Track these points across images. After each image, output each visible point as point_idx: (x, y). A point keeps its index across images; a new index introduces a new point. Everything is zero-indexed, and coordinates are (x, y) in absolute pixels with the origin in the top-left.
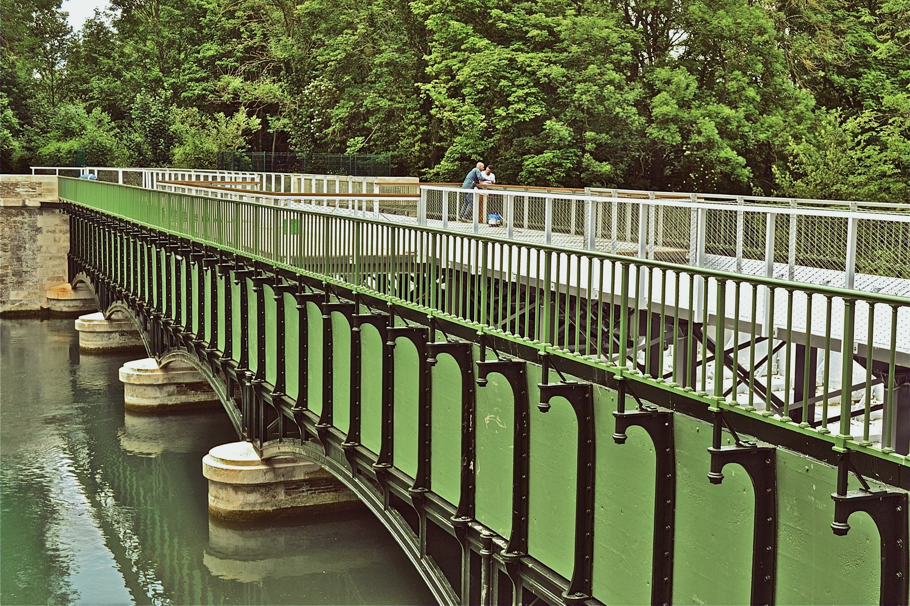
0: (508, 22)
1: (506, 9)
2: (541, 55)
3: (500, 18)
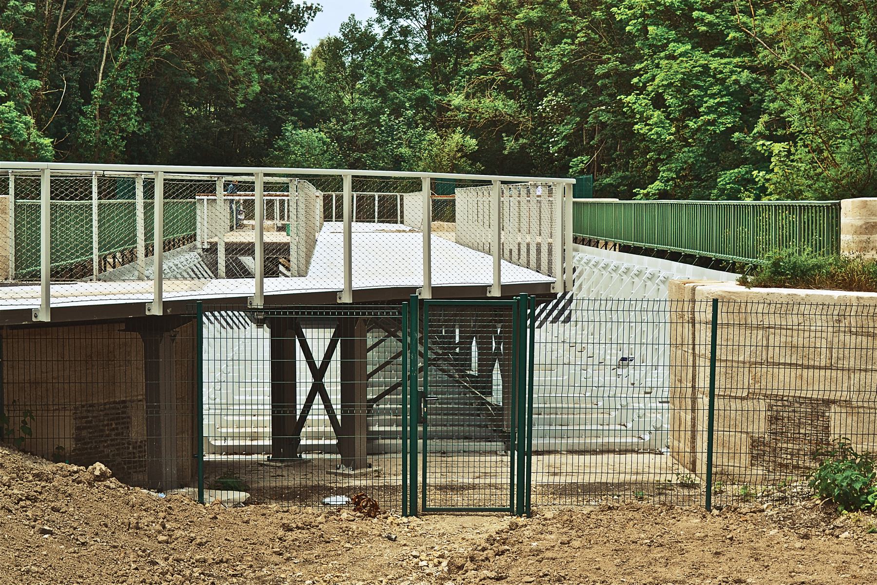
0: (710, 24)
1: (710, 10)
2: (737, 60)
3: (701, 20)
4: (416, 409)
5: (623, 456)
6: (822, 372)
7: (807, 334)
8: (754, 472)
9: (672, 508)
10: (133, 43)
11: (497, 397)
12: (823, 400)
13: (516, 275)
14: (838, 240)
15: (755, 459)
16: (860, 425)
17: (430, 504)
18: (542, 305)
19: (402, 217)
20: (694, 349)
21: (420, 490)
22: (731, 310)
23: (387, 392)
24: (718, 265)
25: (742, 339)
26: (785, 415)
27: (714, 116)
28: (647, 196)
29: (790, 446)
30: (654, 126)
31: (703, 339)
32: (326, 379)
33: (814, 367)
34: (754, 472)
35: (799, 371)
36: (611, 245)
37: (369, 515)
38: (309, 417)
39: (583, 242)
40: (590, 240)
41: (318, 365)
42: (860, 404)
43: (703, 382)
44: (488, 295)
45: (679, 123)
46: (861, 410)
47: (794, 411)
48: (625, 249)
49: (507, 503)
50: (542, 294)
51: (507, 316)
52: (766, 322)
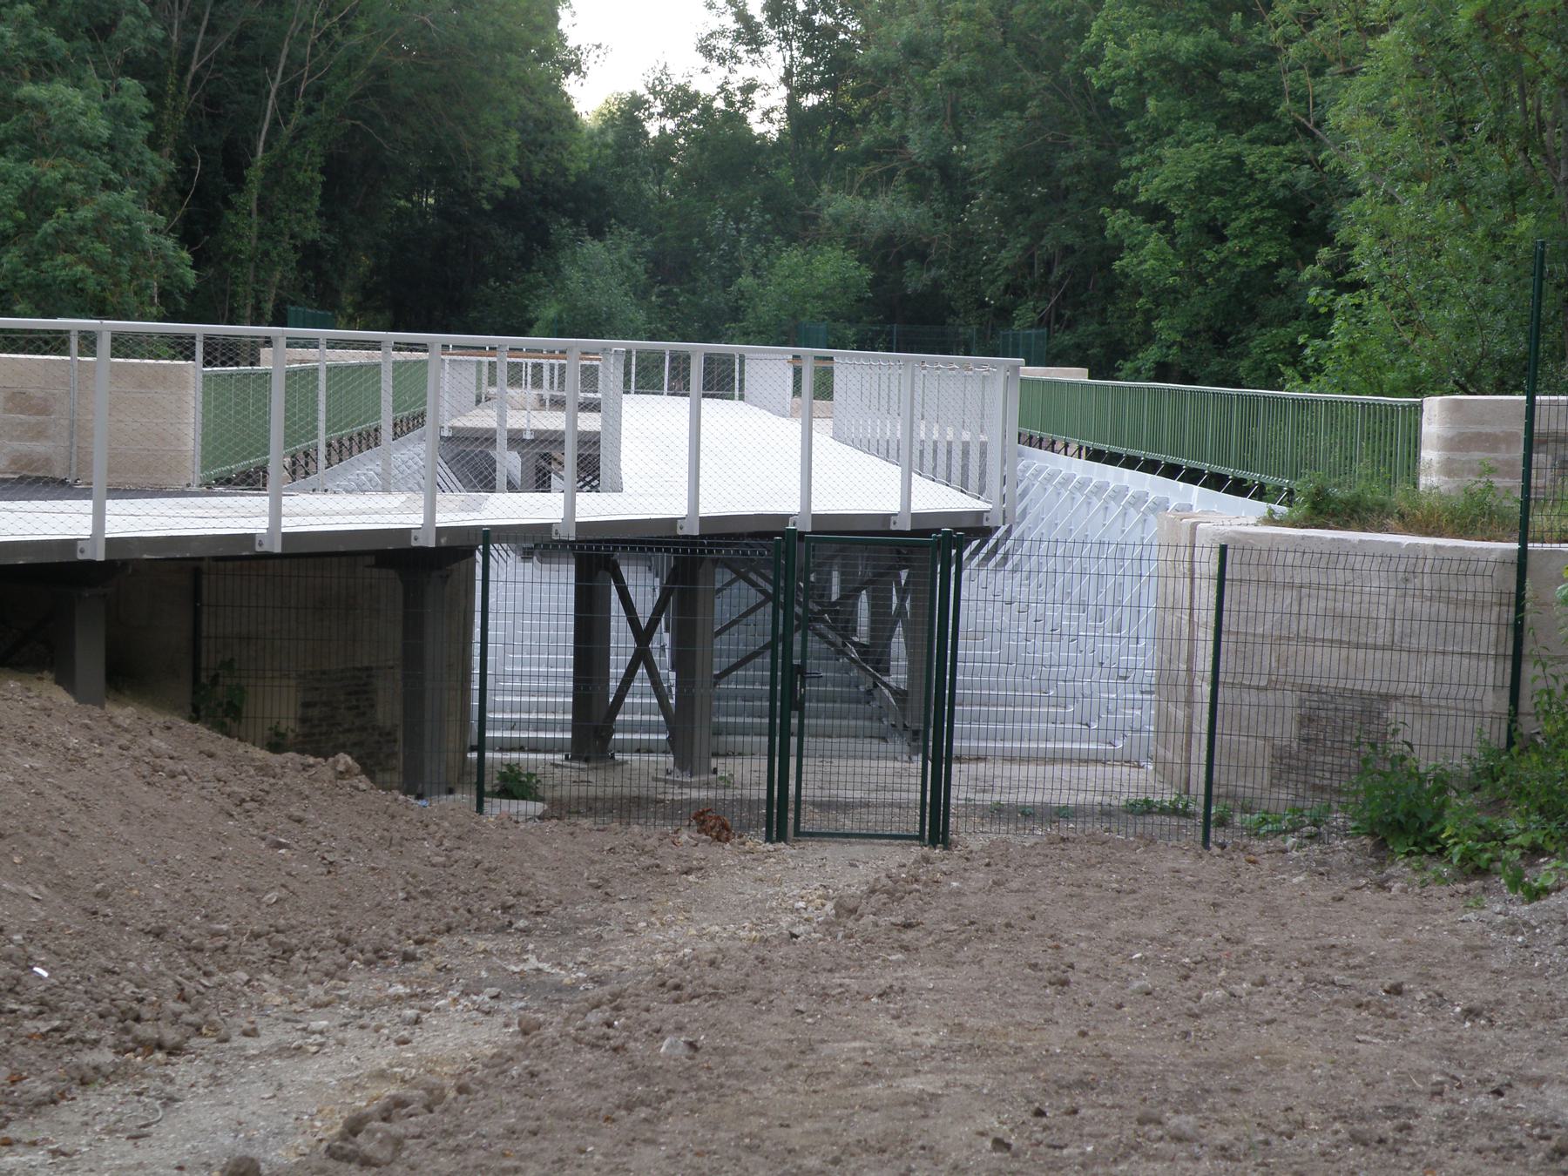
0: (1249, 89)
4: (790, 689)
5: (1083, 769)
6: (1379, 654)
7: (1357, 598)
8: (1275, 796)
9: (1153, 841)
10: (319, 93)
11: (898, 676)
12: (1379, 695)
13: (936, 498)
14: (1417, 455)
15: (1276, 780)
16: (1434, 732)
17: (805, 826)
18: (975, 543)
19: (741, 388)
20: (1191, 615)
21: (792, 806)
22: (1246, 559)
23: (736, 667)
24: (1239, 488)
25: (1261, 602)
26: (1323, 713)
27: (1249, 245)
28: (1136, 375)
29: (1329, 759)
30: (1147, 256)
31: (1204, 600)
32: (654, 645)
33: (1366, 646)
34: (1275, 796)
35: (1344, 652)
36: (1073, 448)
37: (718, 838)
38: (627, 700)
39: (1030, 442)
40: (1041, 440)
41: (644, 623)
42: (1434, 701)
43: (1204, 663)
44: (893, 528)
45: (1190, 254)
46: (1436, 711)
47: (1336, 709)
48: (1096, 456)
49: (915, 829)
50: (974, 530)
51: (919, 560)
52: (1297, 581)
